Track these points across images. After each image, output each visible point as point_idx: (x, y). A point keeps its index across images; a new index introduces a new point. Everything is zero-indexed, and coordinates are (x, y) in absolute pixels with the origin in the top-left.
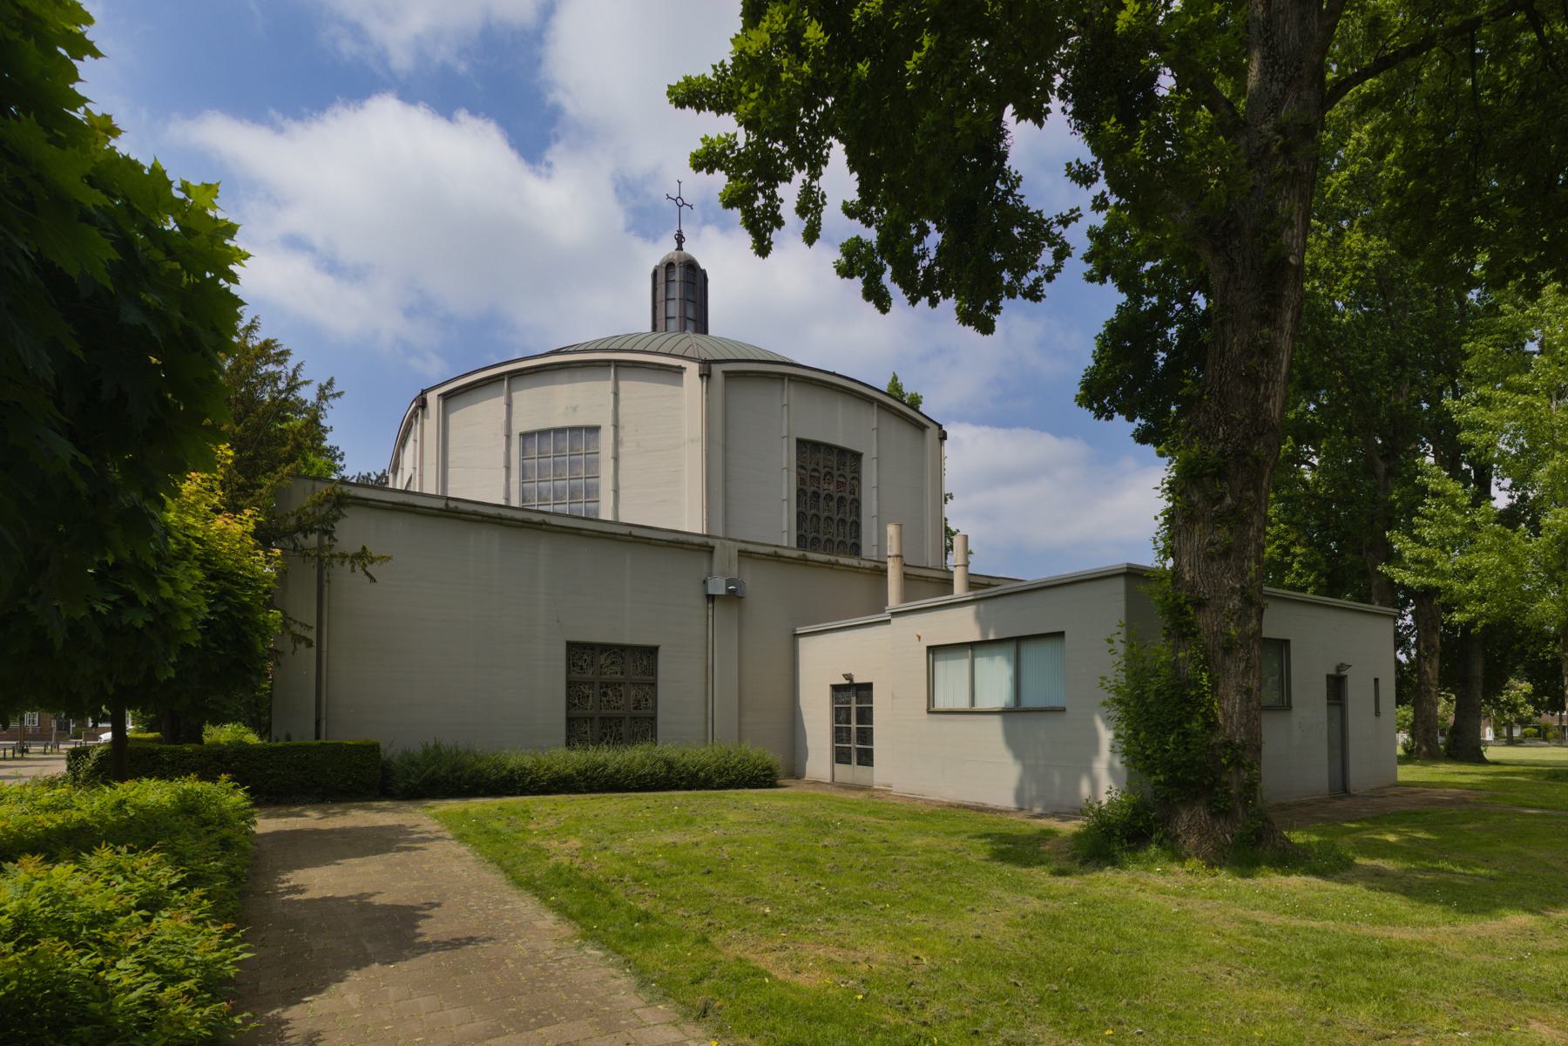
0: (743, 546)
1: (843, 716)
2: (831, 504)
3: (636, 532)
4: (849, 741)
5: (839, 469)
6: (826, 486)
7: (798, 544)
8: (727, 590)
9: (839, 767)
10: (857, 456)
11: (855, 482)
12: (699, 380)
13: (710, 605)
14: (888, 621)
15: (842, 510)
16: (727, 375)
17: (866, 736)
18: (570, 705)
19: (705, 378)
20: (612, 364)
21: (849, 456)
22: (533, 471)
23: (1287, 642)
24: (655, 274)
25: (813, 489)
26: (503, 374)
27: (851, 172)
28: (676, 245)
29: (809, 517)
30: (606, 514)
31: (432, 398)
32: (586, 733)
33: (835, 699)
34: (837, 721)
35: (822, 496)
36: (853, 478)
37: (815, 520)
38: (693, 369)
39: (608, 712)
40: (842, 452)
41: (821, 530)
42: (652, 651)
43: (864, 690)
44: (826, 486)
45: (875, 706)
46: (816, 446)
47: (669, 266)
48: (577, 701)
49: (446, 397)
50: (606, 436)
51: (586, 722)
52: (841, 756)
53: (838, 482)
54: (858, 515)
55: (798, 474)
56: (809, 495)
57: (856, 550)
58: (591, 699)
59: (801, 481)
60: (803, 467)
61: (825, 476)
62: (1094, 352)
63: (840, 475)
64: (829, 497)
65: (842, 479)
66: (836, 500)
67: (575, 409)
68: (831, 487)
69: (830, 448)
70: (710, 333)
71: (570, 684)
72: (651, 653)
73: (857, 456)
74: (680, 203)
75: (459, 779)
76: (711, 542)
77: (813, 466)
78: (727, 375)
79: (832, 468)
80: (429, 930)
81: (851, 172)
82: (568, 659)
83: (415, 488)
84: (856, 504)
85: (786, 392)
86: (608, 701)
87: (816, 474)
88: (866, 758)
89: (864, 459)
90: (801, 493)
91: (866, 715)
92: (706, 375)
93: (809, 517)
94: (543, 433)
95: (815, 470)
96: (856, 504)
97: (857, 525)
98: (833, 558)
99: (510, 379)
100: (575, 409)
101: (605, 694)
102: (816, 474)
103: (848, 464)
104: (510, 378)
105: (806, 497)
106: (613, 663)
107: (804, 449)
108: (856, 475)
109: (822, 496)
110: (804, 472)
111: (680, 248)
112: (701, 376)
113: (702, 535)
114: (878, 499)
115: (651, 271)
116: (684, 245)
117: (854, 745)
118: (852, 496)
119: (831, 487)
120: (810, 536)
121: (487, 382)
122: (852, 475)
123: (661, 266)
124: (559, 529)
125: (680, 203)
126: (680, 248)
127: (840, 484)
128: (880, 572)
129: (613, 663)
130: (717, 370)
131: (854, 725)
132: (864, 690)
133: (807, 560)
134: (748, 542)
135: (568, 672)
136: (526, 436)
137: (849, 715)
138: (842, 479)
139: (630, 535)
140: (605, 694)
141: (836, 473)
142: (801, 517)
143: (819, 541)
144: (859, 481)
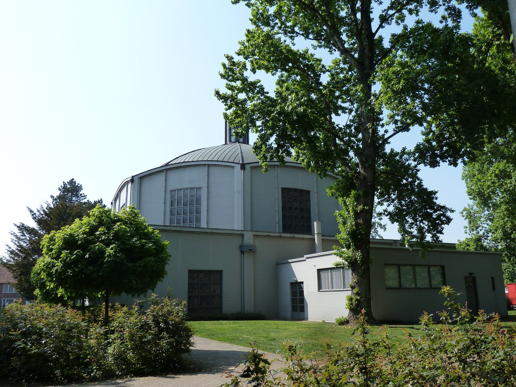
3: (214, 231)
10: (308, 192)
13: (243, 255)
14: (305, 260)
18: (189, 292)
20: (207, 165)
26: (164, 170)
30: (203, 225)
32: (195, 302)
40: (301, 191)
42: (221, 272)
44: (295, 204)
46: (290, 190)
48: (192, 290)
51: (195, 298)
58: (197, 289)
60: (284, 198)
64: (296, 208)
69: (296, 190)
71: (189, 285)
72: (313, 240)
73: (308, 192)
75: (132, 337)
76: (243, 233)
78: (251, 167)
82: (189, 276)
85: (276, 171)
86: (203, 290)
87: (291, 200)
89: (311, 194)
98: (292, 235)
101: (202, 288)
102: (291, 200)
104: (166, 171)
105: (286, 209)
106: (205, 277)
114: (318, 208)
124: (186, 232)
129: (205, 277)
130: (247, 167)
133: (282, 237)
135: (189, 280)
139: (212, 232)
140: (202, 288)
142: (284, 217)
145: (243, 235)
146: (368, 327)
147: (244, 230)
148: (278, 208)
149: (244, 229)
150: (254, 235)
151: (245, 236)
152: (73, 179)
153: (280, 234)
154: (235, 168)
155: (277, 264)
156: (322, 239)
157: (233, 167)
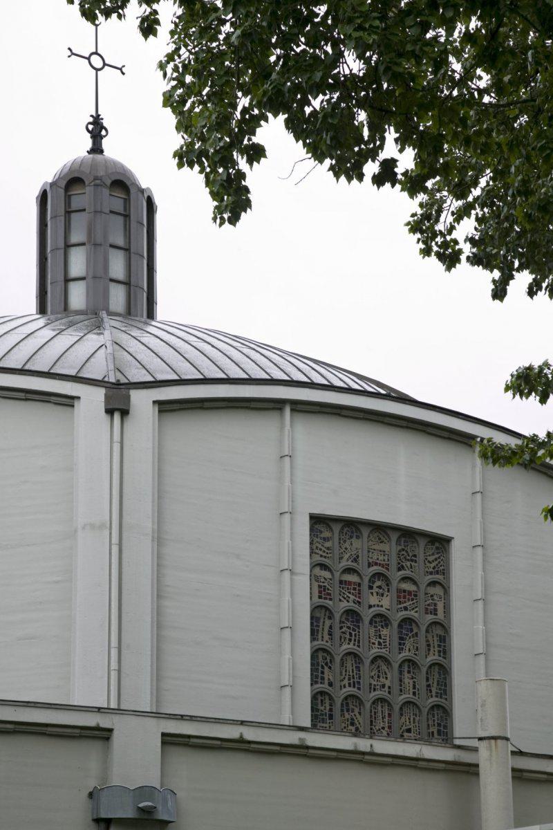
2: (385, 632)
5: (401, 568)
6: (374, 600)
7: (315, 718)
10: (440, 543)
11: (438, 590)
12: (105, 418)
15: (409, 643)
16: (164, 407)
19: (117, 416)
21: (365, 532)
24: (43, 198)
25: (344, 605)
27: (297, 141)
28: (88, 143)
29: (338, 659)
35: (367, 620)
36: (433, 583)
37: (350, 663)
38: (93, 399)
41: (365, 681)
44: (374, 600)
46: (352, 526)
47: (72, 181)
53: (399, 591)
54: (445, 651)
55: (314, 578)
56: (337, 616)
57: (441, 729)
59: (321, 591)
60: (323, 567)
61: (372, 581)
62: (520, 367)
63: (405, 579)
64: (381, 619)
65: (407, 586)
66: (395, 624)
68: (386, 602)
70: (161, 312)
74: (95, 59)
76: (105, 722)
77: (345, 563)
78: (164, 407)
79: (387, 567)
81: (297, 141)
83: (106, 379)
84: (439, 631)
87: (353, 578)
90: (319, 614)
92: (118, 407)
93: (338, 659)
95: (349, 570)
96: (441, 633)
97: (442, 671)
98: (363, 744)
103: (421, 557)
107: (327, 534)
108: (439, 577)
109: (367, 620)
110: (327, 574)
111: (97, 149)
112: (110, 412)
115: (36, 192)
116: (106, 143)
118: (430, 617)
119: (386, 602)
120: (340, 694)
121: (318, 408)
122: (430, 578)
123: (53, 185)
125: (95, 59)
126: (97, 149)
127: (402, 595)
130: (142, 402)
138: (407, 586)
141: (395, 576)
143: (361, 703)
144: (446, 590)
145: (103, 735)
146: (140, 19)
147: (119, 711)
148: (294, 667)
149: (119, 704)
150: (169, 740)
151: (117, 737)
152: (449, 269)
153: (302, 735)
154: (80, 407)
155: (281, 457)
156: (513, 770)
157: (68, 401)
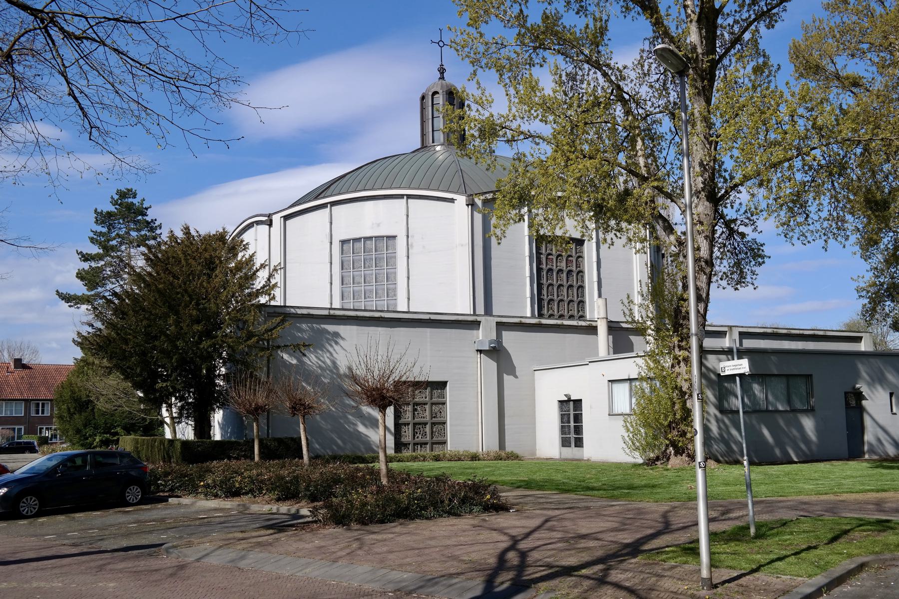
0: (499, 320)
1: (566, 419)
3: (433, 317)
4: (569, 433)
8: (490, 347)
9: (565, 449)
13: (479, 356)
15: (570, 279)
17: (578, 430)
22: (383, 293)
23: (811, 375)
24: (423, 98)
31: (276, 219)
33: (561, 409)
34: (562, 422)
38: (461, 200)
39: (419, 419)
42: (581, 400)
43: (578, 403)
45: (584, 412)
49: (286, 218)
50: (401, 243)
52: (565, 443)
61: (557, 258)
67: (379, 225)
80: (507, 378)
88: (579, 443)
91: (578, 418)
94: (357, 240)
99: (331, 206)
100: (379, 225)
111: (442, 78)
113: (470, 315)
115: (420, 96)
117: (573, 436)
126: (442, 78)
128: (592, 330)
131: (572, 424)
132: (578, 403)
134: (502, 317)
136: (343, 242)
137: (569, 418)
